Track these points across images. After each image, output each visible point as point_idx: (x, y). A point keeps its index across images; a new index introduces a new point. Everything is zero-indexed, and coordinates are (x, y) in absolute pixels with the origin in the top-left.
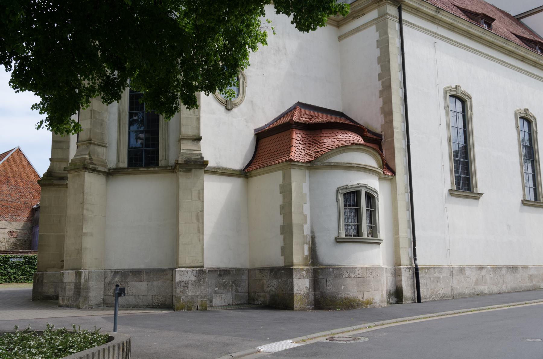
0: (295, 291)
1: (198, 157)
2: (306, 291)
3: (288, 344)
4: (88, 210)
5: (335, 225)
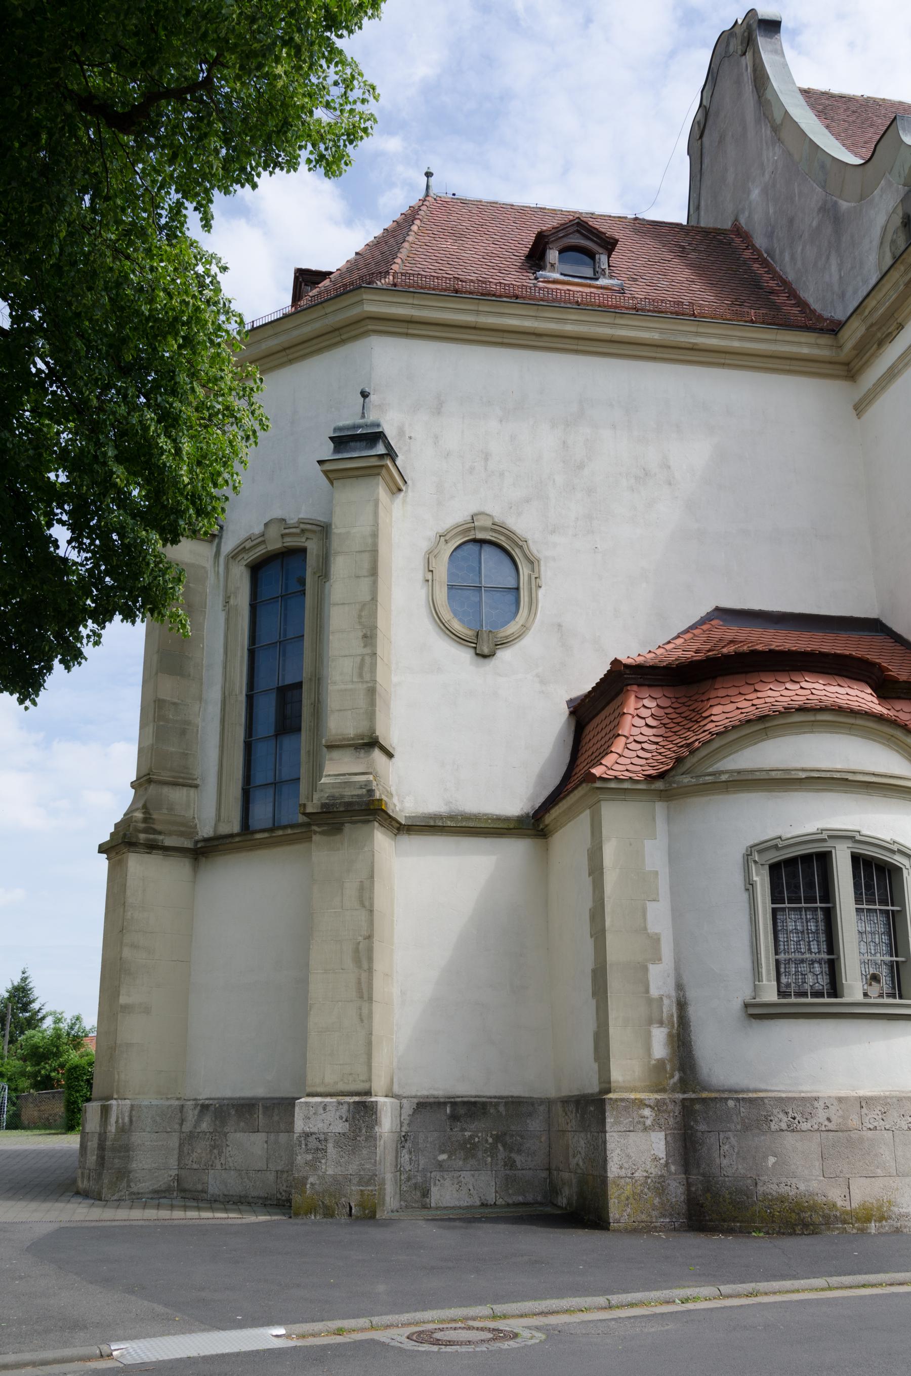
0: (613, 1170)
1: (360, 792)
2: (654, 1171)
3: (272, 1336)
4: (134, 946)
5: (744, 962)
